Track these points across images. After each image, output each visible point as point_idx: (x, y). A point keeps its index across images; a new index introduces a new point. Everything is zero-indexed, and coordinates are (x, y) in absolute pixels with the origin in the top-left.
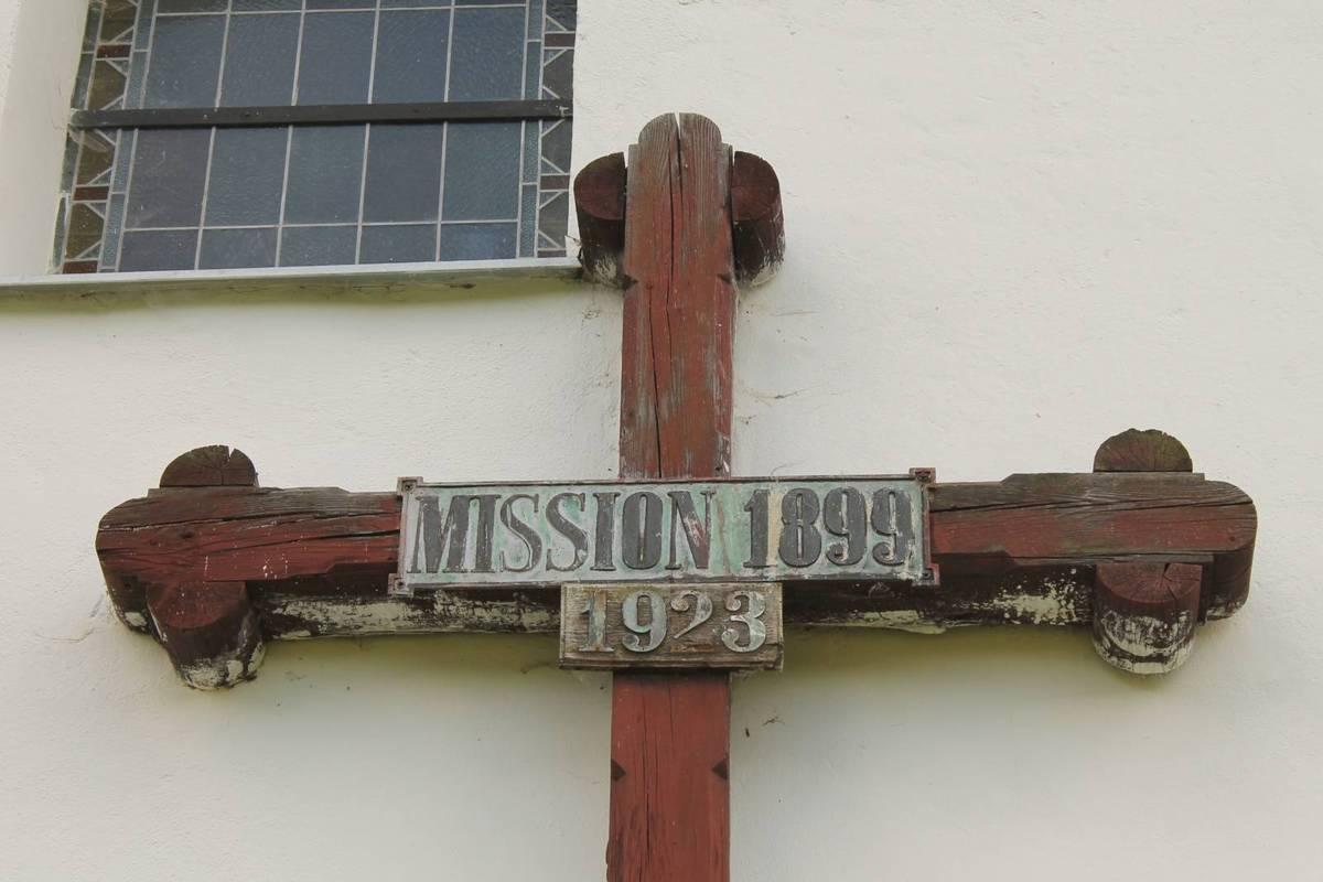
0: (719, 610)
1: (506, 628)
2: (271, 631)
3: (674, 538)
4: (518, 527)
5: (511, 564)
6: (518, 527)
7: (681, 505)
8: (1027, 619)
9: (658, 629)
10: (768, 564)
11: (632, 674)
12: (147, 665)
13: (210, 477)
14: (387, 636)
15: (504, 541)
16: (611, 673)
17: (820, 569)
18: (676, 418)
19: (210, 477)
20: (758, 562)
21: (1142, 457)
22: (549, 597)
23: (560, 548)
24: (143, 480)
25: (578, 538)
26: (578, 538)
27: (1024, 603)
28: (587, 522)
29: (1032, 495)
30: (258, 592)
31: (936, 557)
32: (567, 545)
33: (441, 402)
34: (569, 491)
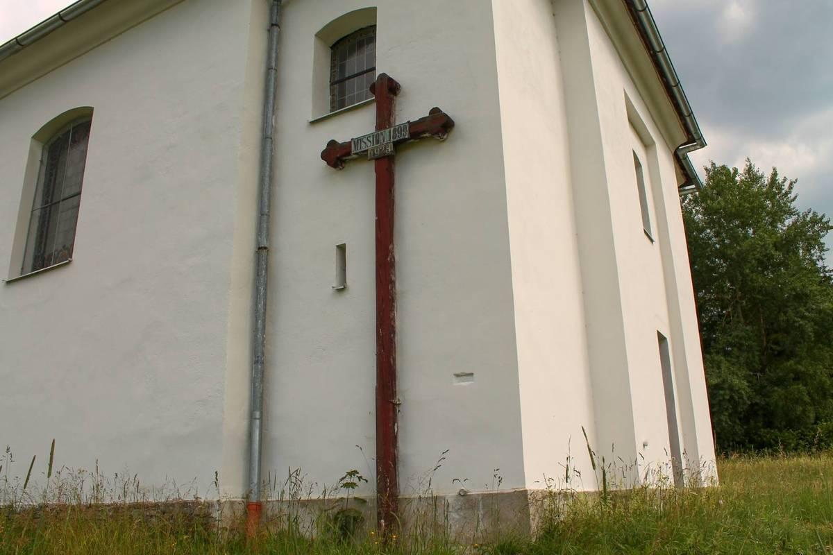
0: (385, 148)
1: (363, 156)
2: (344, 161)
3: (381, 138)
4: (364, 142)
5: (364, 147)
6: (364, 142)
7: (382, 133)
8: (427, 137)
9: (378, 153)
10: (431, 496)
11: (377, 159)
12: (333, 169)
13: (332, 144)
14: (262, 201)
15: (363, 145)
16: (374, 161)
17: (397, 139)
18: (384, 119)
19: (332, 144)
20: (390, 140)
21: (435, 111)
22: (367, 151)
23: (369, 144)
24: (324, 147)
25: (370, 142)
26: (370, 142)
27: (425, 135)
28: (371, 140)
29: (422, 120)
30: (338, 158)
31: (410, 133)
32: (369, 143)
33: (356, 126)
34: (369, 136)
